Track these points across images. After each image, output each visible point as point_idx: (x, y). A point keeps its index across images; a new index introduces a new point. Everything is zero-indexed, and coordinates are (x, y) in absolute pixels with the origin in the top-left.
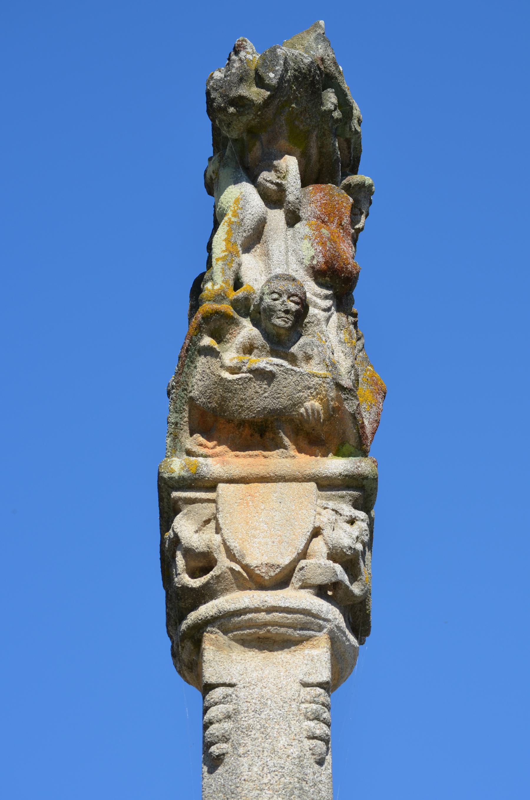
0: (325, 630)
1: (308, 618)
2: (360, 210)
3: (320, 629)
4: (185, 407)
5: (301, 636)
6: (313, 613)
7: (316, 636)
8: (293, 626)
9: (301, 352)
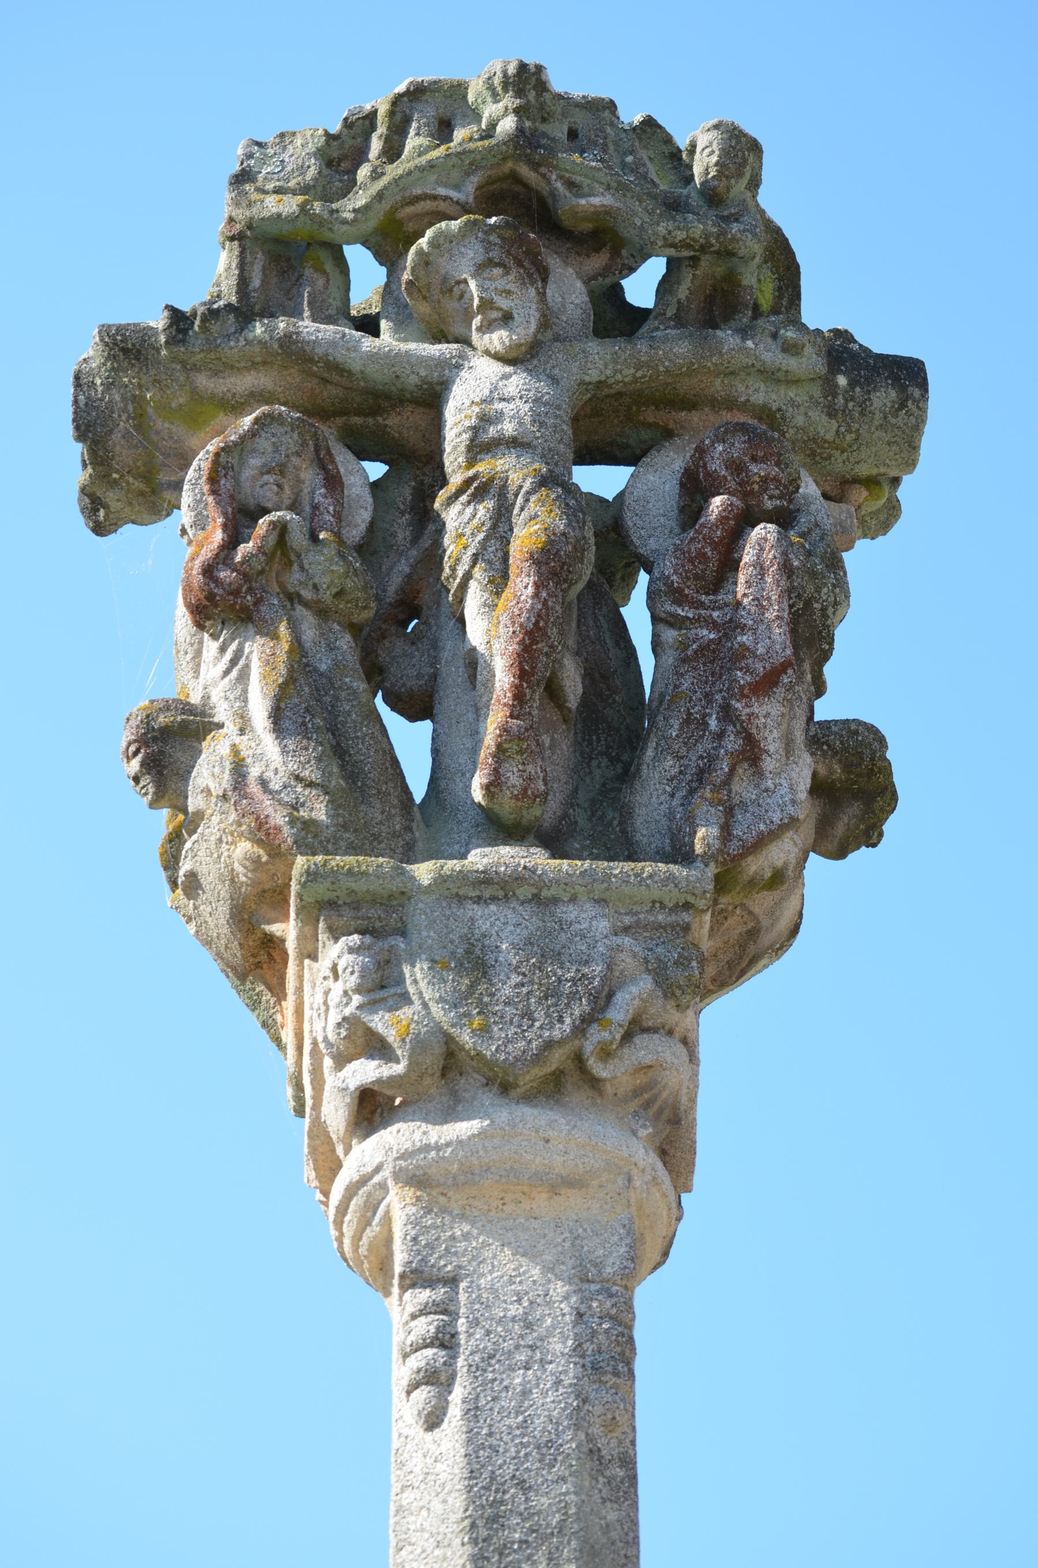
0: (390, 1183)
1: (360, 1192)
2: (458, 282)
3: (383, 1187)
4: (257, 990)
5: (380, 1224)
6: (358, 1182)
7: (389, 1205)
8: (365, 1223)
9: (199, 797)
